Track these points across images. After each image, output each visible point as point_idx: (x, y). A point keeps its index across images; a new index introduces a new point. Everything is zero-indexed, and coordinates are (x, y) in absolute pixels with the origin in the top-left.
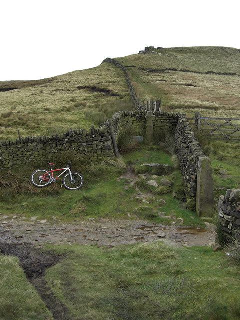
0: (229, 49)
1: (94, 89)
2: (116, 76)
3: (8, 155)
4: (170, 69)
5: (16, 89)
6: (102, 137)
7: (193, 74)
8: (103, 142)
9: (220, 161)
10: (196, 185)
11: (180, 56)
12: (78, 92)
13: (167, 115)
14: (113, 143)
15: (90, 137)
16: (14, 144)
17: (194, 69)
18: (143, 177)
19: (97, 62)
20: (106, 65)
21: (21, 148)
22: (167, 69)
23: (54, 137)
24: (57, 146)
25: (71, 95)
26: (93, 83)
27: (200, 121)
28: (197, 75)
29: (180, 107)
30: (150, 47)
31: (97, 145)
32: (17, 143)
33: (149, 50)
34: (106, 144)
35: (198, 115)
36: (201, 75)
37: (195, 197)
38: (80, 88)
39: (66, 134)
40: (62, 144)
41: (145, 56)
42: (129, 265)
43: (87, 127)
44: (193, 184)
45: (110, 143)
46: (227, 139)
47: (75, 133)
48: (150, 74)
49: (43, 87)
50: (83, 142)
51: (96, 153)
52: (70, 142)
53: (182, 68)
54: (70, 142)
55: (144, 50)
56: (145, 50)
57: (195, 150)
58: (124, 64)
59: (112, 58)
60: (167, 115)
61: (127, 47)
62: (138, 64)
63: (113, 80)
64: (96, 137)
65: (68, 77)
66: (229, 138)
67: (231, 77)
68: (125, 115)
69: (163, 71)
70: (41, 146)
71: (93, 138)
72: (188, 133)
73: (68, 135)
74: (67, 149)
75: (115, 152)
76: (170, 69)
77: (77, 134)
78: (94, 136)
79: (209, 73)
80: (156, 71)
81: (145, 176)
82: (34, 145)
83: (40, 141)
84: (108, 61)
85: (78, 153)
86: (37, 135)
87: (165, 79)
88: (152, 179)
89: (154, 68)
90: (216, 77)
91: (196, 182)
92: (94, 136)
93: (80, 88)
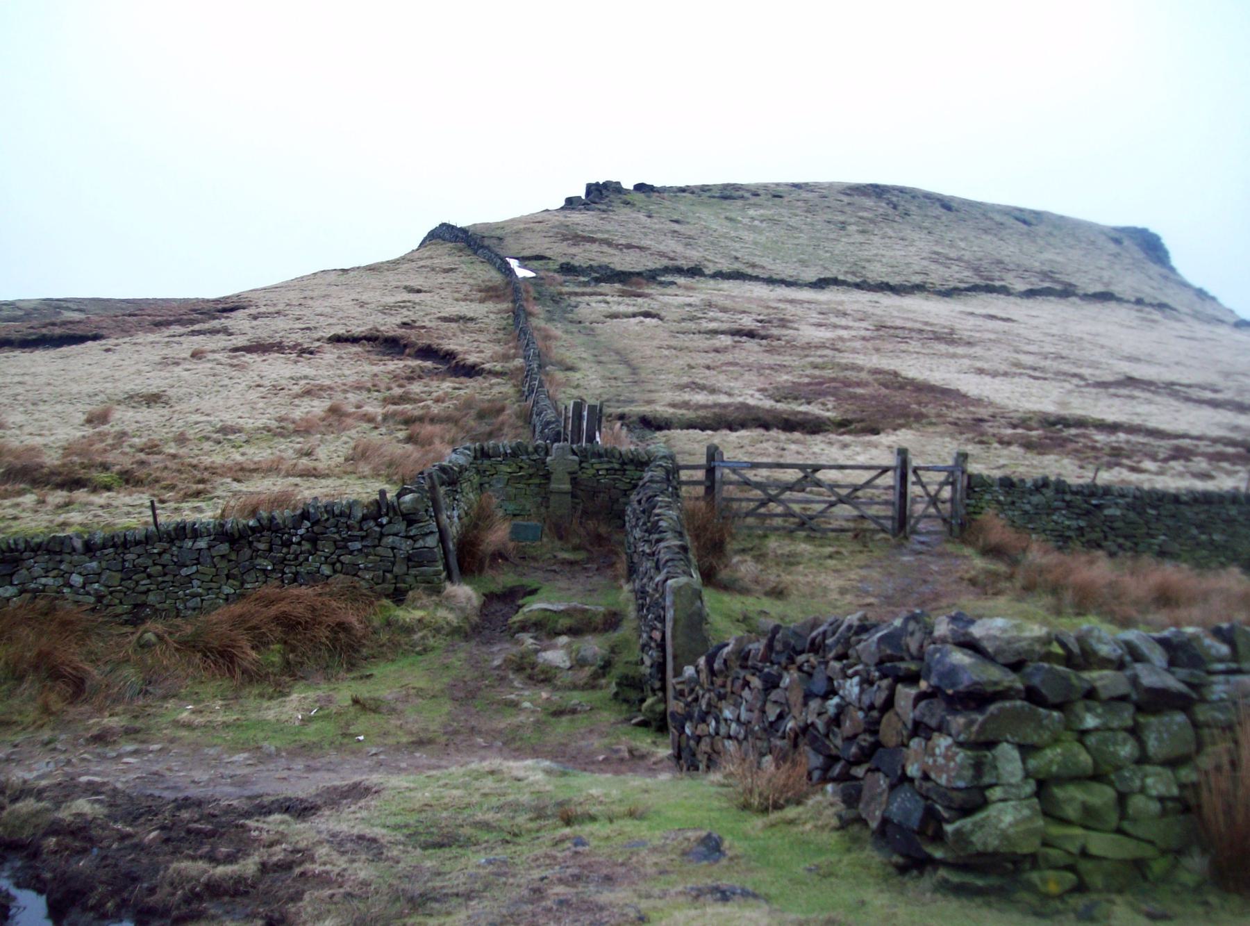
0: (902, 190)
1: (391, 345)
3: (119, 576)
4: (679, 271)
5: (95, 338)
10: (664, 657)
11: (710, 218)
12: (331, 354)
13: (617, 455)
14: (443, 539)
15: (372, 523)
16: (138, 543)
18: (528, 640)
19: (404, 239)
20: (444, 256)
21: (160, 554)
23: (265, 522)
24: (271, 550)
25: (304, 368)
26: (389, 325)
30: (606, 185)
31: (393, 548)
32: (148, 539)
33: (601, 194)
34: (420, 543)
35: (713, 453)
37: (663, 689)
38: (337, 340)
39: (298, 512)
40: (287, 544)
41: (582, 220)
43: (362, 490)
44: (654, 653)
45: (431, 541)
46: (807, 526)
47: (327, 512)
49: (200, 332)
50: (353, 539)
51: (391, 572)
52: (313, 539)
53: (725, 266)
54: (313, 539)
55: (582, 193)
56: (588, 193)
57: (667, 561)
60: (617, 455)
61: (518, 187)
64: (390, 522)
68: (483, 454)
70: (224, 548)
71: (382, 526)
72: (658, 515)
73: (305, 515)
74: (301, 559)
75: (447, 567)
77: (334, 516)
81: (535, 638)
82: (202, 544)
83: (222, 534)
84: (445, 234)
85: (335, 571)
86: (205, 514)
88: (554, 647)
91: (662, 646)
92: (385, 520)
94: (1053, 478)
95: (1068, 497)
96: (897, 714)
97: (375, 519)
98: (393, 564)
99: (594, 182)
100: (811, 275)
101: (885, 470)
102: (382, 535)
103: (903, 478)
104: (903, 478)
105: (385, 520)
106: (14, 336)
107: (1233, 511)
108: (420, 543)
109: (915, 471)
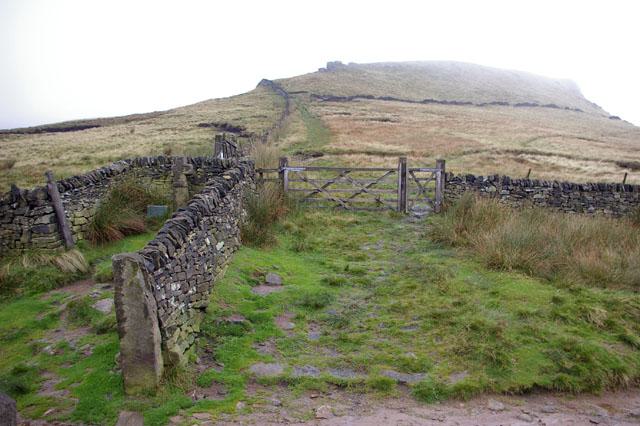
2: (271, 106)
4: (363, 97)
5: (97, 127)
6: (32, 208)
7: (399, 104)
8: (32, 217)
9: (293, 253)
15: (7, 207)
17: (404, 95)
19: (249, 85)
22: (357, 96)
27: (286, 173)
28: (409, 105)
29: (351, 152)
34: (38, 221)
36: (414, 105)
38: (201, 125)
42: (422, 368)
45: (45, 220)
48: (328, 103)
53: (382, 94)
55: (325, 67)
58: (288, 89)
59: (270, 79)
61: (295, 63)
62: (311, 88)
63: (263, 112)
64: (18, 206)
65: (192, 109)
66: (347, 205)
67: (460, 107)
69: (350, 99)
76: (363, 97)
78: (15, 205)
79: (425, 102)
80: (338, 99)
84: (265, 81)
87: (349, 111)
89: (335, 94)
90: (436, 107)
93: (201, 125)
94: (501, 176)
95: (510, 188)
96: (138, 345)
97: (9, 204)
98: (21, 234)
99: (333, 60)
100: (422, 98)
101: (392, 171)
102: (14, 216)
103: (404, 175)
104: (404, 175)
105: (15, 205)
106: (60, 133)
107: (617, 196)
108: (38, 221)
109: (411, 172)
